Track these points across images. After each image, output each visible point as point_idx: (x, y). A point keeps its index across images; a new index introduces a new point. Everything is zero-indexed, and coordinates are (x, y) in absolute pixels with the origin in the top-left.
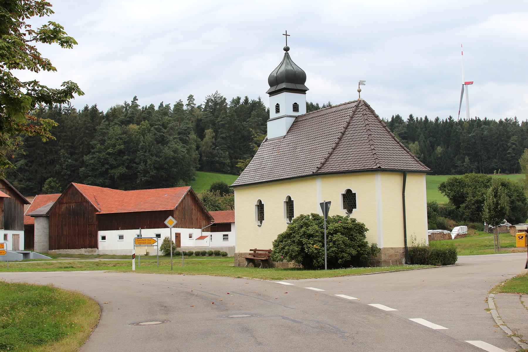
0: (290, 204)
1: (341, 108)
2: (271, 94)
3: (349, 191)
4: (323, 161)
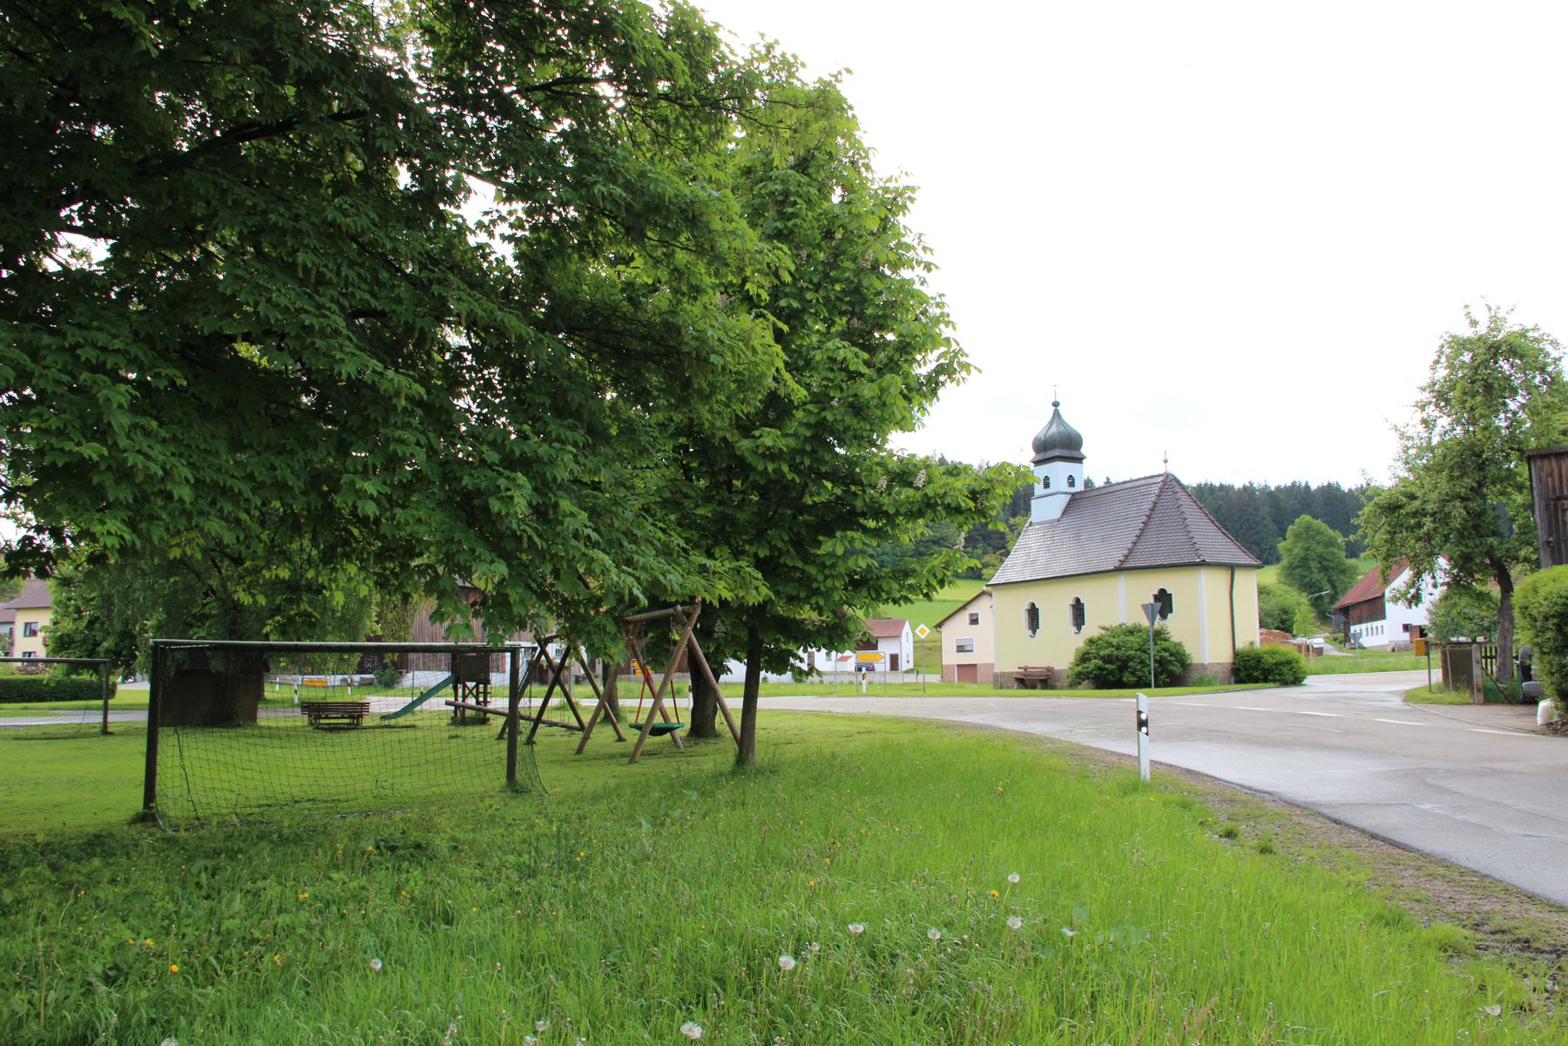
0: (1078, 611)
1: (1138, 483)
2: (1037, 463)
3: (1162, 591)
4: (1126, 552)
